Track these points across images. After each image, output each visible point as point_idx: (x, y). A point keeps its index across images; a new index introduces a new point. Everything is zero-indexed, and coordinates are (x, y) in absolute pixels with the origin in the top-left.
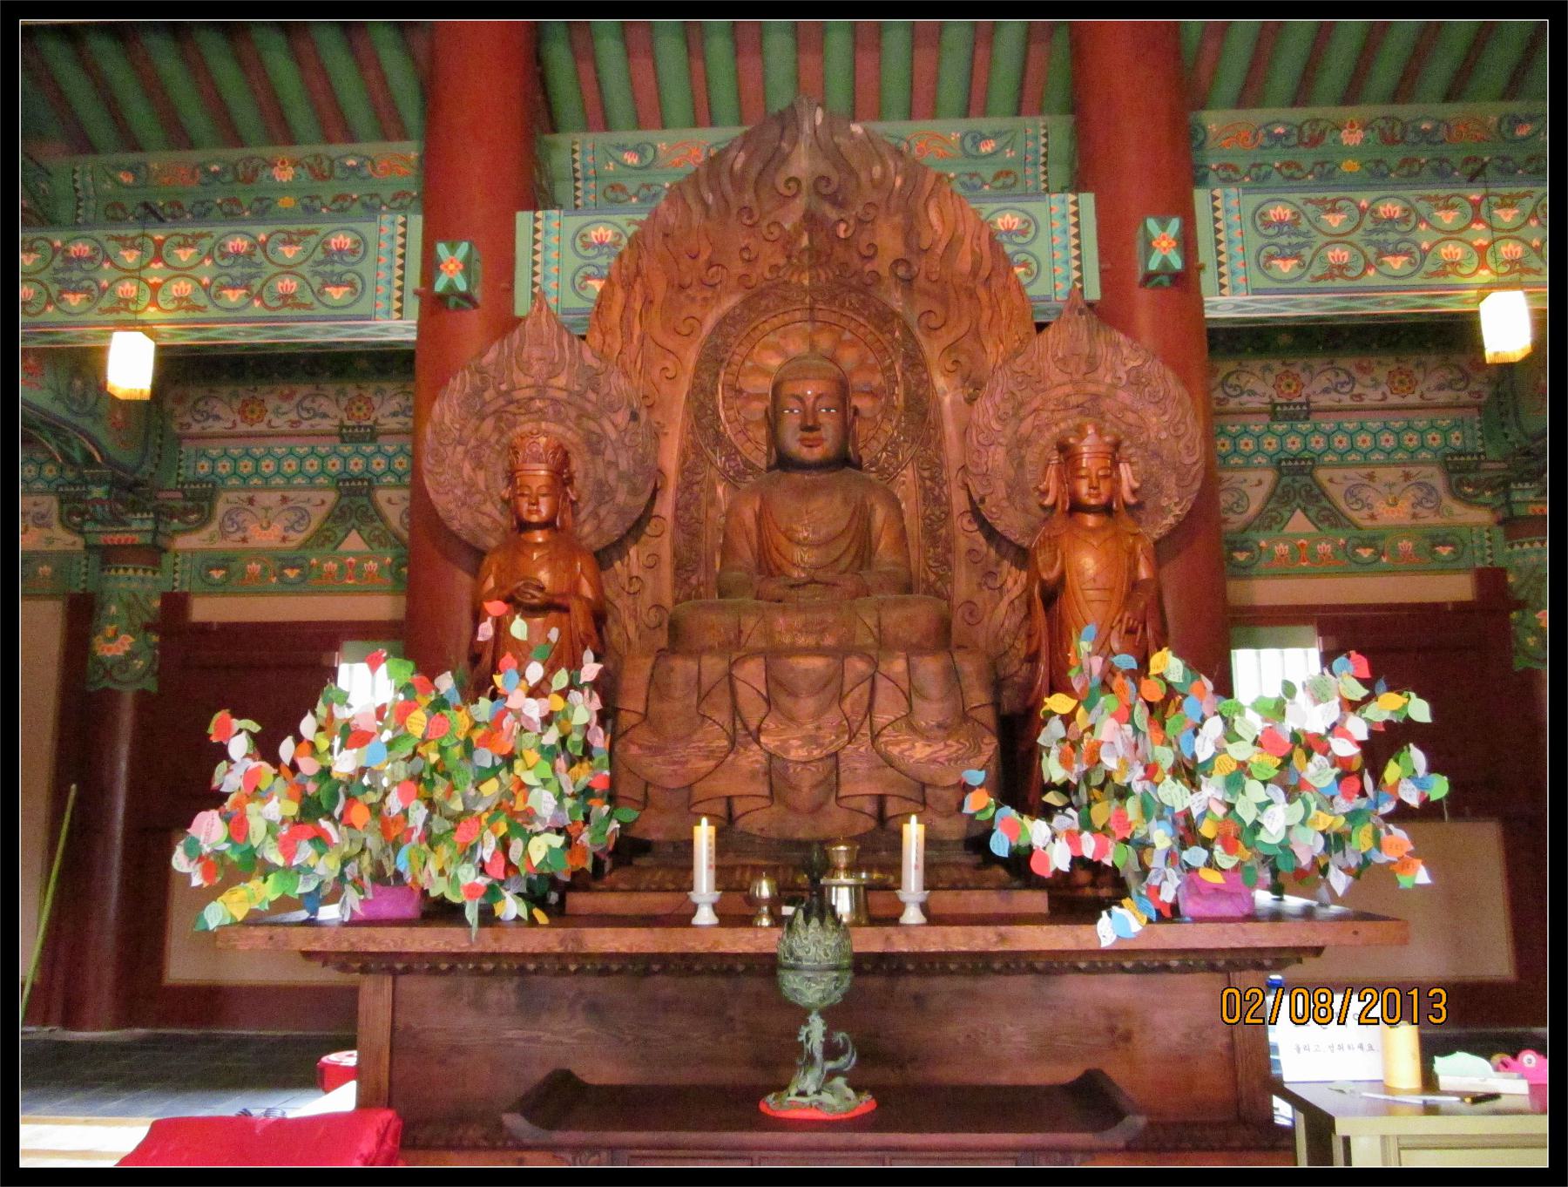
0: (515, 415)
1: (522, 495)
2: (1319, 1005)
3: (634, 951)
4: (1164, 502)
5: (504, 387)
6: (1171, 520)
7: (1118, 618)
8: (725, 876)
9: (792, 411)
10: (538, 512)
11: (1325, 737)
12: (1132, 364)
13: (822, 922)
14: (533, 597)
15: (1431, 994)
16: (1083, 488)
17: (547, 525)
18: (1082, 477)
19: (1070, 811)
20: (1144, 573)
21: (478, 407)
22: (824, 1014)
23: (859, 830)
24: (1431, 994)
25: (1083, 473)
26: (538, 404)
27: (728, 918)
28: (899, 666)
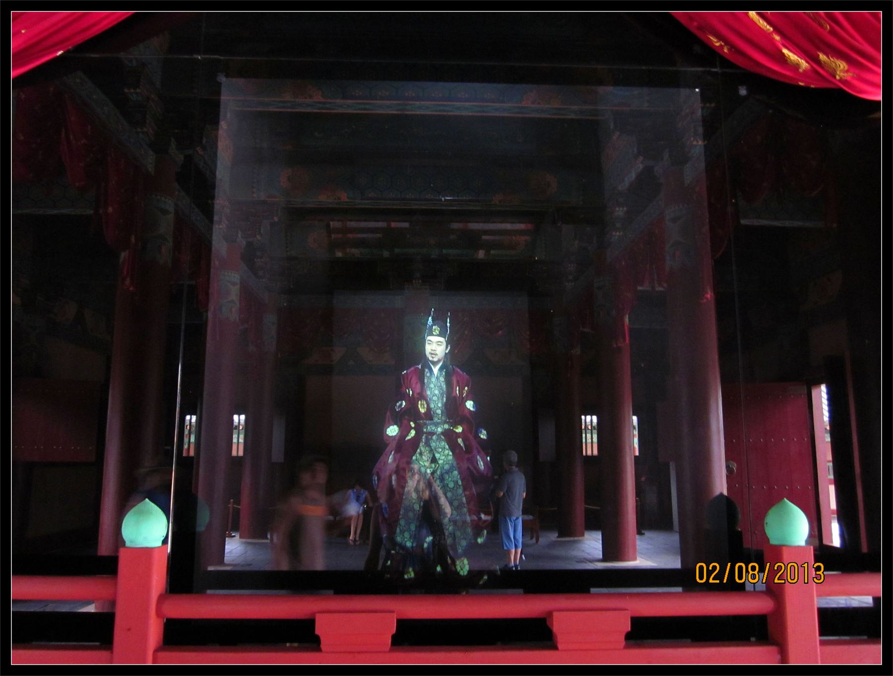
2: (751, 572)
15: (776, 568)
24: (776, 568)
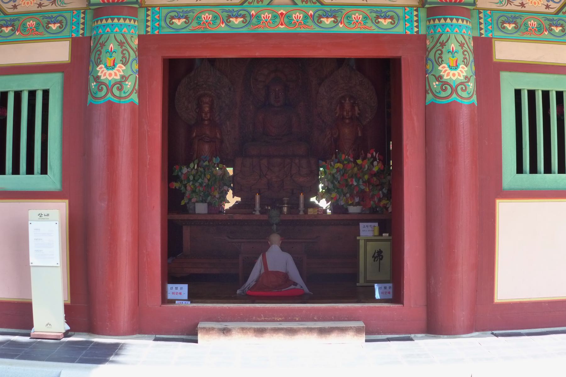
0: (198, 89)
1: (203, 112)
3: (244, 219)
4: (367, 115)
5: (196, 82)
6: (368, 120)
7: (352, 146)
8: (262, 205)
9: (272, 94)
10: (207, 117)
11: (208, 203)
12: (360, 79)
13: (274, 210)
14: (207, 139)
16: (345, 113)
17: (209, 120)
18: (345, 111)
19: (201, 197)
20: (360, 135)
21: (208, 117)
22: (276, 224)
23: (176, 188)
25: (345, 110)
26: (204, 86)
27: (262, 213)
28: (297, 161)
